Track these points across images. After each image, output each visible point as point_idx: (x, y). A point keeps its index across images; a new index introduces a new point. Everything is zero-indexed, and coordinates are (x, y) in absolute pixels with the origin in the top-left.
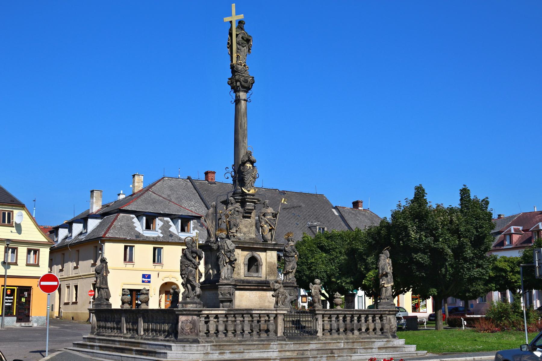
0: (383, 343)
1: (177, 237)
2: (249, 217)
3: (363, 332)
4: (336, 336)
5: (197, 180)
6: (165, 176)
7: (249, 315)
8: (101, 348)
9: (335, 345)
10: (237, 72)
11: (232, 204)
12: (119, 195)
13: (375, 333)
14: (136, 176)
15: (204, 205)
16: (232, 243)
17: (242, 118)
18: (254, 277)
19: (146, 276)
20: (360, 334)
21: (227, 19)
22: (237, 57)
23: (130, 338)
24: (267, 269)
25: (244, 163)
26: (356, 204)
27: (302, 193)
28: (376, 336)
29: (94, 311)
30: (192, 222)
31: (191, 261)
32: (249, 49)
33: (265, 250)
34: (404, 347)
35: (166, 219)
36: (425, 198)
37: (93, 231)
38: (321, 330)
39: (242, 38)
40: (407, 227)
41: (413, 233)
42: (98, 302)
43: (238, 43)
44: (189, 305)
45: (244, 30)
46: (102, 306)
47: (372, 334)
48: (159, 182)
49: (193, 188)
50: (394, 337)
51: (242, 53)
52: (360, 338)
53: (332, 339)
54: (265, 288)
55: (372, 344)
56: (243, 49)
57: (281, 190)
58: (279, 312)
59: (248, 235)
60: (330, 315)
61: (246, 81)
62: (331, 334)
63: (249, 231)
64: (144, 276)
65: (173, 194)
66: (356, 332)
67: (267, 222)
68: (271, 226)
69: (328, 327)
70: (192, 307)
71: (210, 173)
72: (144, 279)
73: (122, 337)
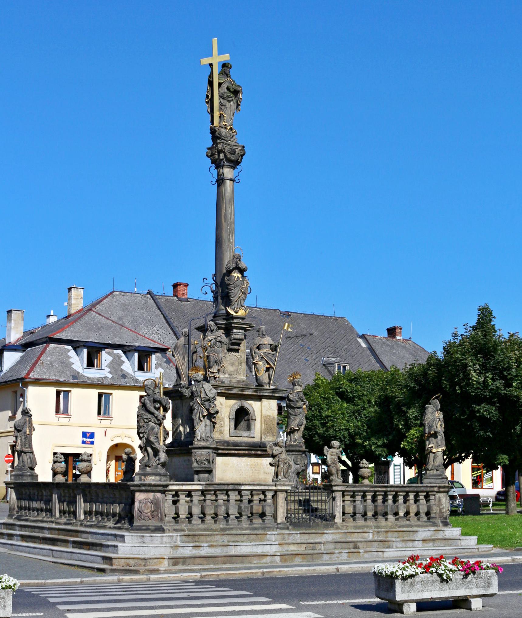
0: (429, 533)
1: (132, 378)
2: (237, 351)
3: (401, 518)
4: (361, 522)
5: (162, 296)
6: (114, 290)
7: (237, 492)
8: (23, 538)
9: (360, 535)
10: (219, 138)
11: (212, 331)
12: (48, 316)
13: (419, 519)
14: (73, 289)
15: (171, 332)
16: (211, 387)
17: (228, 206)
18: (243, 437)
19: (88, 435)
20: (397, 520)
21: (206, 61)
22: (220, 117)
23: (65, 524)
24: (263, 425)
25: (229, 272)
26: (392, 332)
27: (314, 315)
28: (419, 523)
29: (12, 486)
30: (154, 356)
31: (153, 414)
32: (238, 105)
33: (260, 398)
34: (460, 539)
35: (116, 352)
36: (492, 323)
37: (11, 369)
38: (340, 514)
39: (228, 89)
40: (465, 366)
41: (474, 374)
42: (18, 472)
43: (221, 97)
44: (149, 478)
45: (230, 77)
46: (25, 478)
47: (413, 520)
48: (107, 299)
49: (156, 307)
50: (446, 524)
51: (228, 111)
52: (396, 525)
53: (356, 527)
54: (259, 452)
55: (413, 535)
56: (228, 104)
57: (283, 310)
58: (279, 488)
59: (235, 376)
60: (354, 492)
61: (233, 152)
62: (354, 520)
63: (237, 370)
64: (84, 435)
65: (126, 316)
66: (391, 517)
67: (263, 357)
68: (268, 363)
69: (350, 510)
70: (153, 480)
71: (180, 285)
72: (85, 439)
73: (52, 522)
